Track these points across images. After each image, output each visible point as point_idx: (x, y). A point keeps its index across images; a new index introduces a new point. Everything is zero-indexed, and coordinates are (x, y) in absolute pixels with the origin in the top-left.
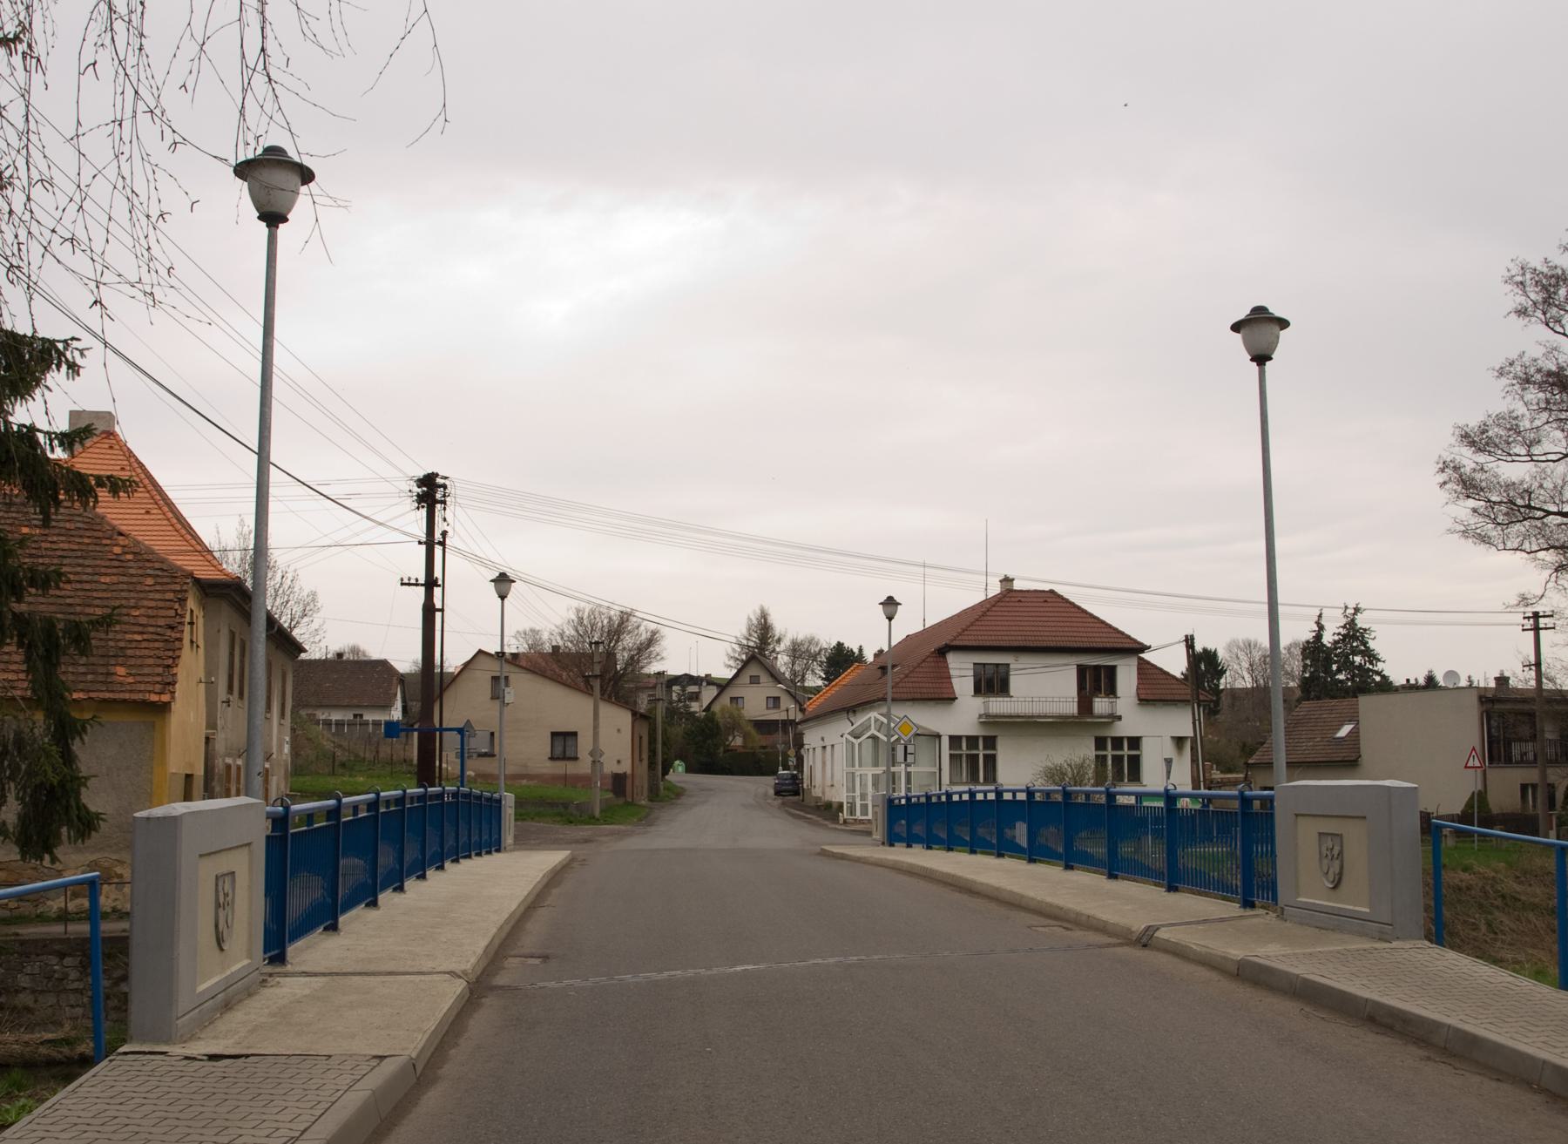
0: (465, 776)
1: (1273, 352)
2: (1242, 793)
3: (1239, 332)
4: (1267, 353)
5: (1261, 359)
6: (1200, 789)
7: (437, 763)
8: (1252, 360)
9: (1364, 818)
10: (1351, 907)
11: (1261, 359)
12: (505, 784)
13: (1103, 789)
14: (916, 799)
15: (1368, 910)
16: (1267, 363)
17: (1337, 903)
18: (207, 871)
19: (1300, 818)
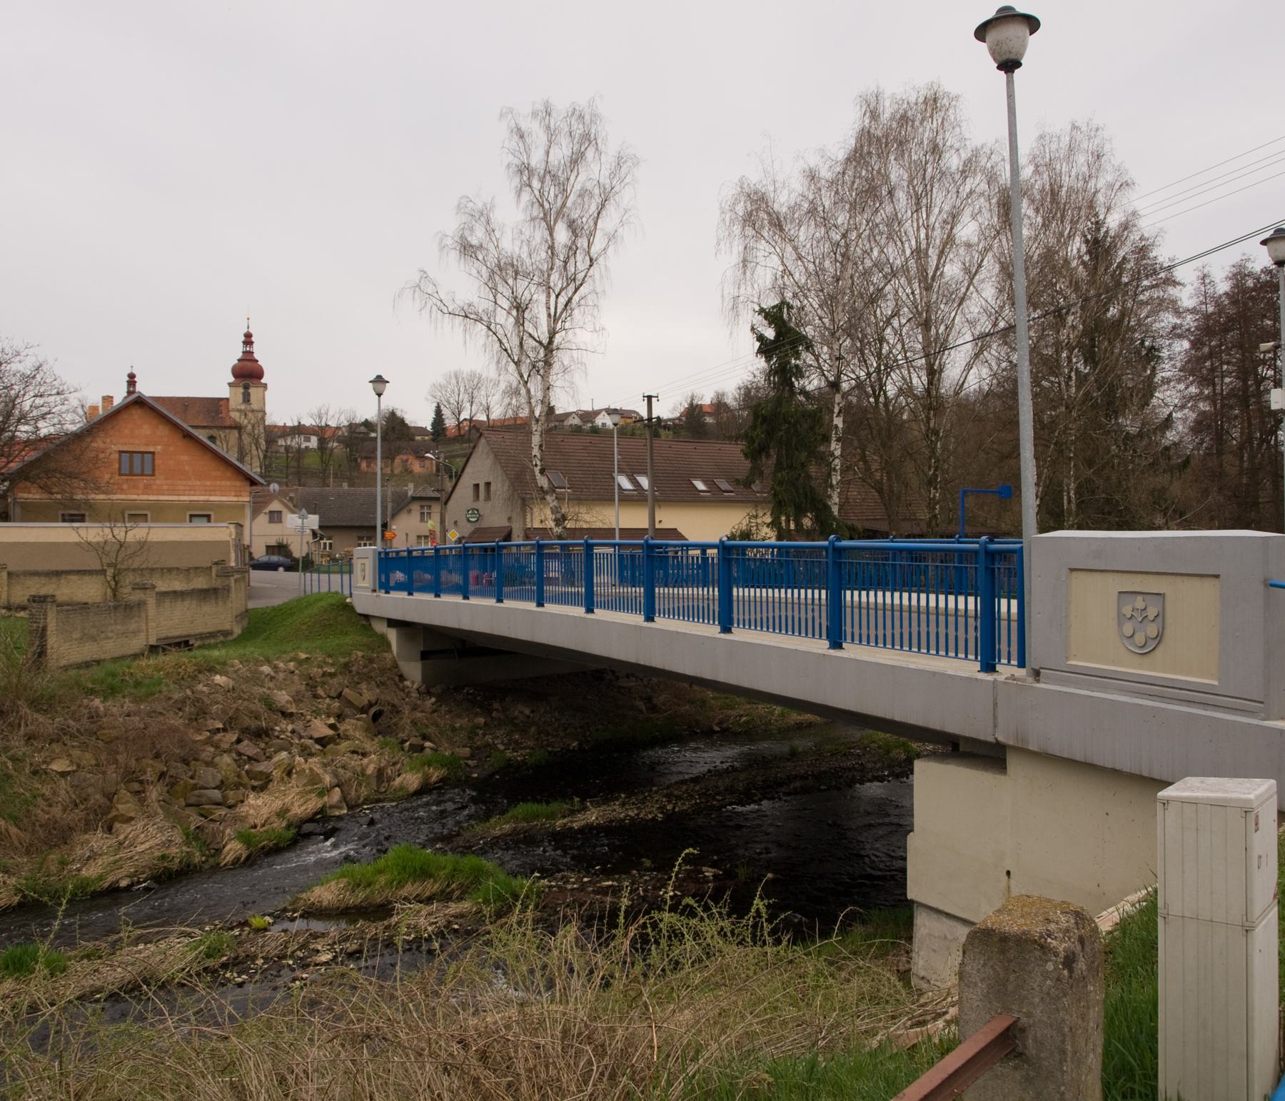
0: (265, 559)
1: (1022, 55)
2: (586, 541)
3: (984, 41)
4: (1012, 57)
5: (1009, 65)
6: (614, 538)
7: (979, 635)
8: (999, 68)
9: (1217, 576)
10: (176, 498)
11: (1009, 65)
12: (637, 1050)
13: (826, 543)
14: (698, 552)
15: (1216, 683)
16: (1016, 71)
17: (1187, 675)
18: (360, 561)
19: (1075, 574)
